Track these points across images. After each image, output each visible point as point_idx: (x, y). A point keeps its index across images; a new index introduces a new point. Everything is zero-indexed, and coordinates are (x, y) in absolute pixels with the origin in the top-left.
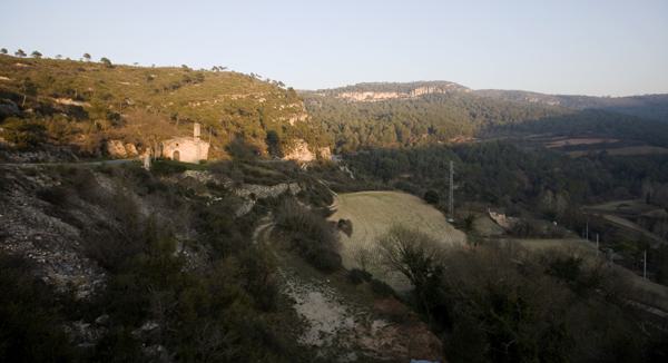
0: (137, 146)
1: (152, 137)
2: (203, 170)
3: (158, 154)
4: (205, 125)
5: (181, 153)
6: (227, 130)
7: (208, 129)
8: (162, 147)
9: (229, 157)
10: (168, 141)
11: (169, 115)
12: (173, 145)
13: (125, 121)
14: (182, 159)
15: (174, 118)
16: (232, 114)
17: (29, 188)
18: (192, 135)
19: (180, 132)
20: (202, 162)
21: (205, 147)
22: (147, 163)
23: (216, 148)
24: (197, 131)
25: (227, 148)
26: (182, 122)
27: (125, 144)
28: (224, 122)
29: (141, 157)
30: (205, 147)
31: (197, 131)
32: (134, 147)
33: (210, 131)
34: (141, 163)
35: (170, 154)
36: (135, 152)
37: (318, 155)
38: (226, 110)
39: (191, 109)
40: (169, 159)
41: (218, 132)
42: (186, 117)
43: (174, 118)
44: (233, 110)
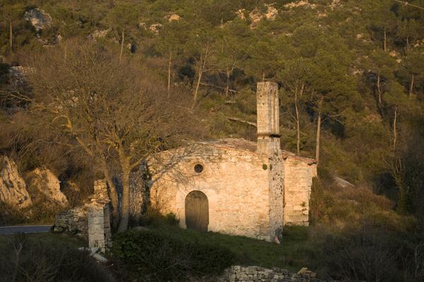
0: (65, 177)
1: (113, 139)
2: (292, 265)
3: (132, 202)
4: (299, 94)
5: (212, 197)
6: (385, 111)
7: (310, 110)
8: (147, 176)
9: (394, 217)
10: (165, 156)
11: (168, 62)
12: (185, 168)
13: (26, 88)
14: (218, 222)
15: (186, 73)
16: (399, 44)
17: (406, 20)
18: (250, 133)
19: (206, 122)
20: (289, 233)
21: (299, 177)
22: (97, 234)
23: (342, 183)
24: (267, 115)
25: (385, 184)
26: (216, 82)
27: (27, 169)
28: (369, 79)
29: (79, 212)
30: (299, 177)
31: (267, 115)
32: (54, 182)
33: (316, 119)
34: (78, 234)
35: (174, 201)
36: (60, 196)
37: (246, 15)
38: (376, 31)
39: (242, 34)
40: (172, 220)
41: (348, 116)
42: (228, 65)
43: (186, 73)
44: (403, 29)
